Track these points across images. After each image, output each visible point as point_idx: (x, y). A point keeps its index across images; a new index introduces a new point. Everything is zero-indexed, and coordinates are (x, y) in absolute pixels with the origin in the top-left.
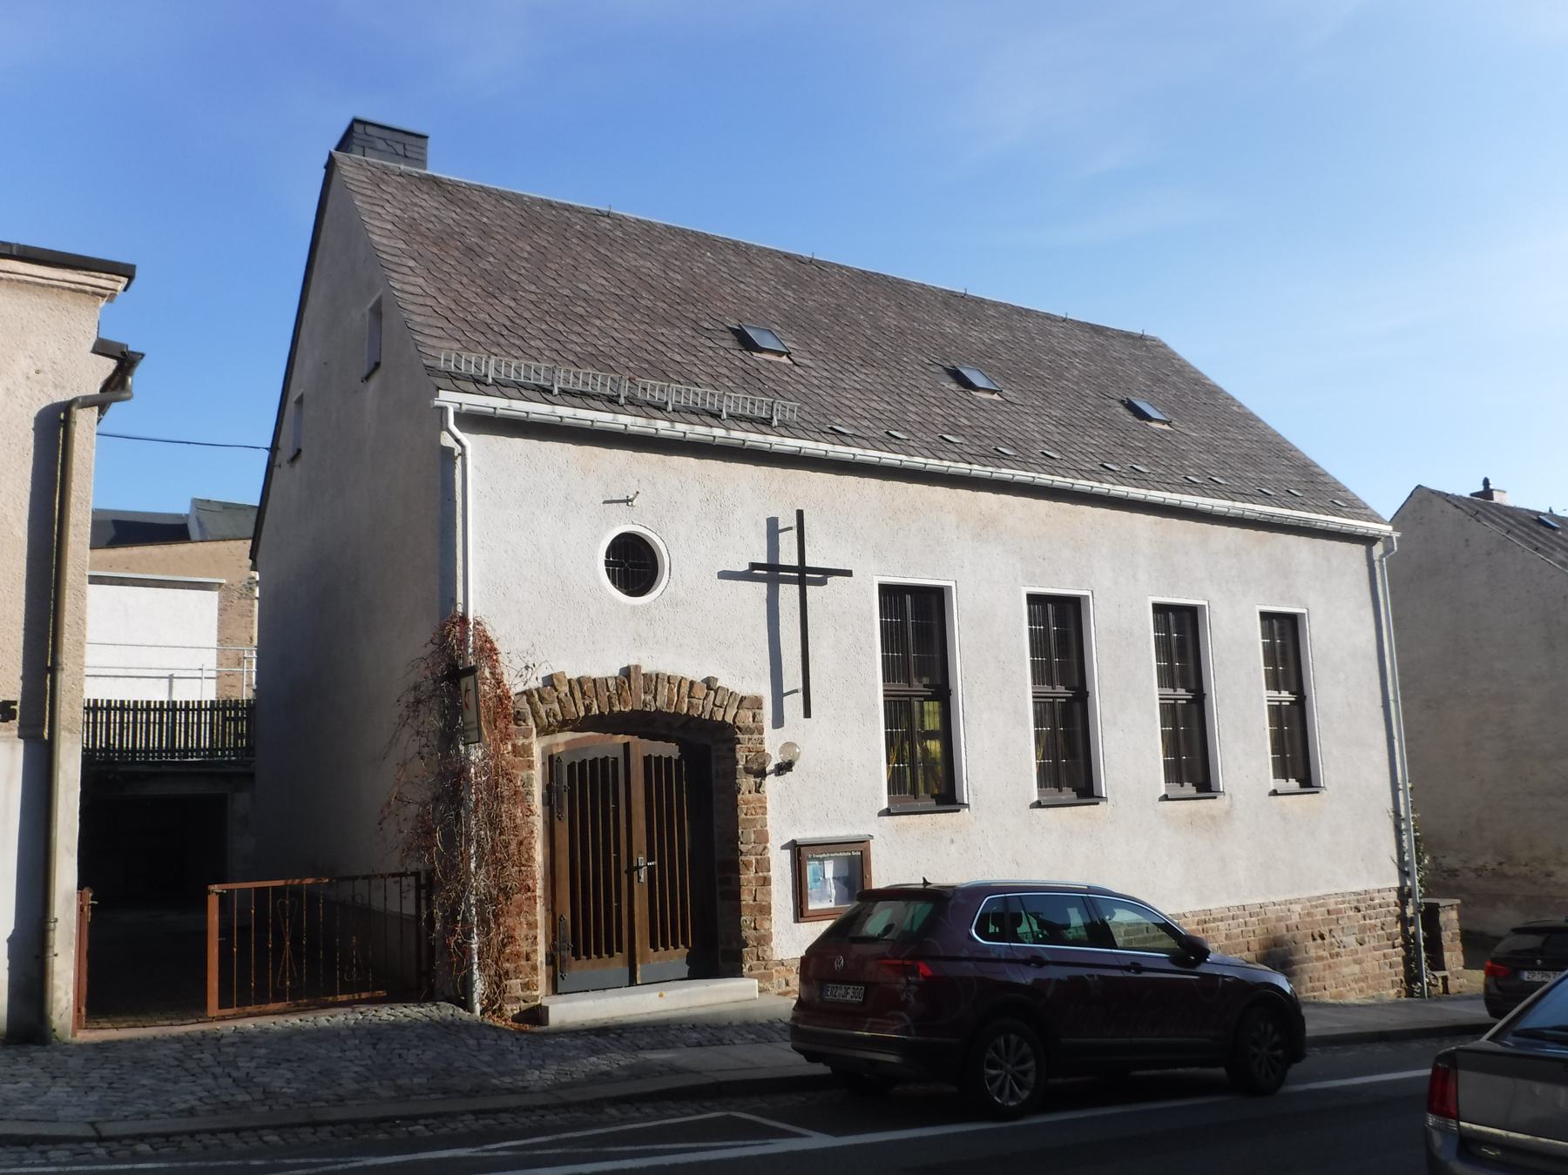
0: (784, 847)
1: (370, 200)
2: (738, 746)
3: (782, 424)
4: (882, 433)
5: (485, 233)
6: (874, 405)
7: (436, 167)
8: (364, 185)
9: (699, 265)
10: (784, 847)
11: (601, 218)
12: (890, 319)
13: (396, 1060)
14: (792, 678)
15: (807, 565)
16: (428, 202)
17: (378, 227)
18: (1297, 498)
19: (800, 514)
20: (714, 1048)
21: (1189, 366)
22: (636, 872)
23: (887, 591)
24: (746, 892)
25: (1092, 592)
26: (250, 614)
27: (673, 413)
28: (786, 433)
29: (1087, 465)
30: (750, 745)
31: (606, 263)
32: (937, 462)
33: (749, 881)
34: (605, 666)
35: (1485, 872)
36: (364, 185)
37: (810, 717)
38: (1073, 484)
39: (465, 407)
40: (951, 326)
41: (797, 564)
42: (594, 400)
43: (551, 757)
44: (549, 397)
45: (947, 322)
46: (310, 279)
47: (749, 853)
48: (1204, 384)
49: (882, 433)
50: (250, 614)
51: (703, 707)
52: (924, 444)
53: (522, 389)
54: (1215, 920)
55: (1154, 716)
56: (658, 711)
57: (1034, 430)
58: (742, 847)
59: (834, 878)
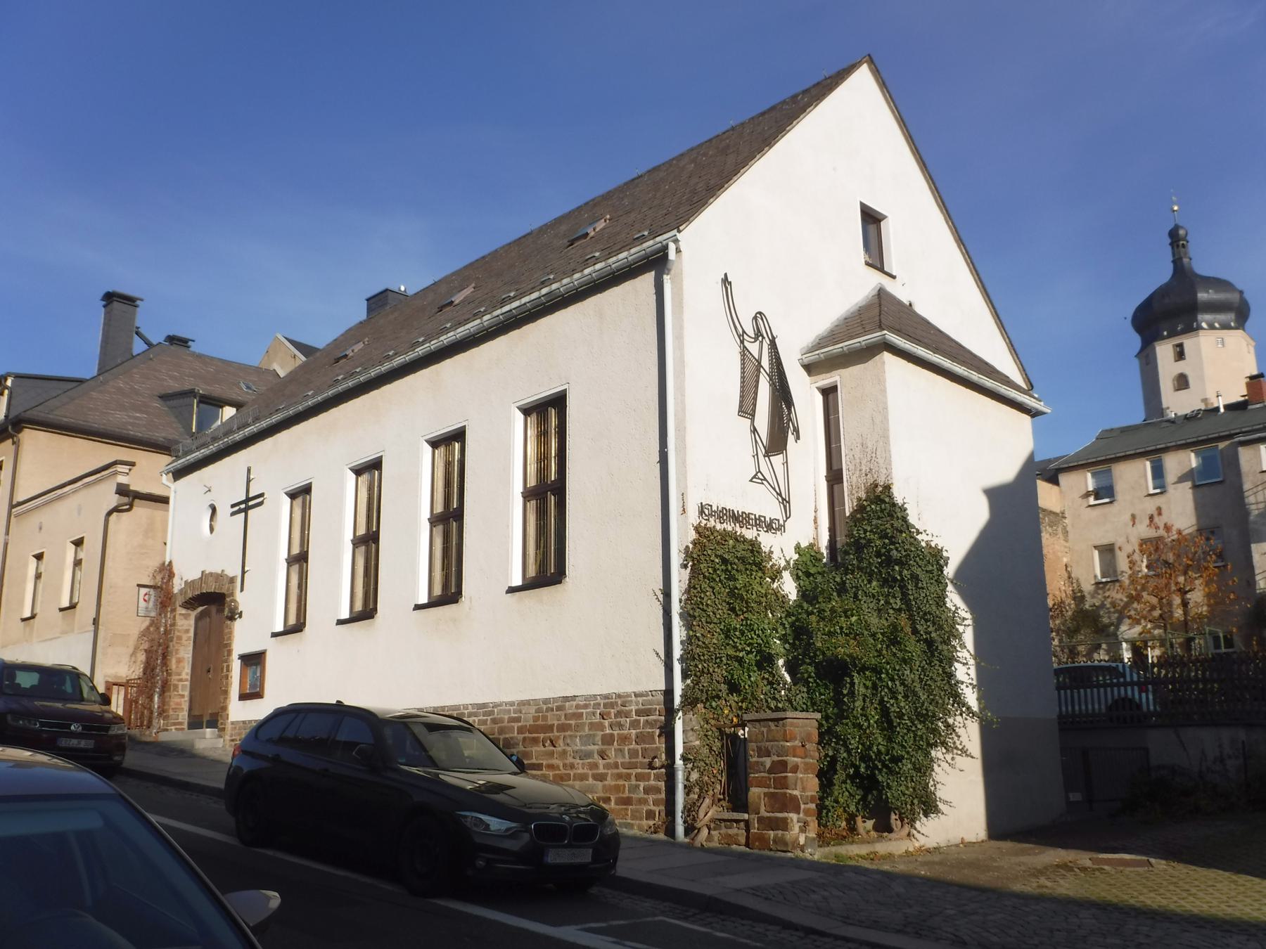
41: (1036, 460)
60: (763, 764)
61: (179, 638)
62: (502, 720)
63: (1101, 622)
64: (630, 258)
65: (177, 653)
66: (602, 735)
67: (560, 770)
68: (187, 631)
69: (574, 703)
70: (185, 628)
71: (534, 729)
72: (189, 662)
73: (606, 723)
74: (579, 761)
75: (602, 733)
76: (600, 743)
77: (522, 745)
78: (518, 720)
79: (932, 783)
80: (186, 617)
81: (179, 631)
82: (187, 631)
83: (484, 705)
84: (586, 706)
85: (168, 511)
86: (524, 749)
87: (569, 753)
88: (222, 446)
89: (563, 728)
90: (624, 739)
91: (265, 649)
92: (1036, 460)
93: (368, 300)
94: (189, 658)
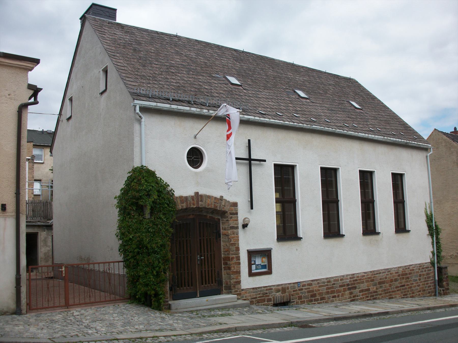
1: (101, 32)
4: (274, 113)
5: (139, 43)
6: (270, 103)
7: (120, 19)
8: (98, 27)
9: (208, 54)
11: (174, 37)
12: (270, 72)
13: (131, 321)
15: (252, 158)
16: (119, 33)
17: (105, 42)
18: (403, 136)
20: (227, 317)
21: (365, 89)
23: (275, 165)
26: (33, 168)
27: (208, 107)
28: (245, 114)
29: (339, 124)
31: (177, 53)
35: (453, 256)
36: (98, 27)
37: (253, 209)
40: (290, 75)
41: (248, 158)
42: (183, 103)
44: (169, 102)
45: (289, 74)
46: (75, 58)
48: (370, 96)
49: (274, 113)
50: (33, 168)
52: (288, 117)
57: (321, 112)
60: (445, 277)
62: (393, 273)
63: (178, 207)
71: (403, 275)
73: (419, 271)
79: (86, 266)
83: (388, 269)
84: (415, 267)
85: (276, 198)
89: (410, 274)
90: (423, 275)
91: (246, 252)
92: (248, 158)
93: (435, 129)
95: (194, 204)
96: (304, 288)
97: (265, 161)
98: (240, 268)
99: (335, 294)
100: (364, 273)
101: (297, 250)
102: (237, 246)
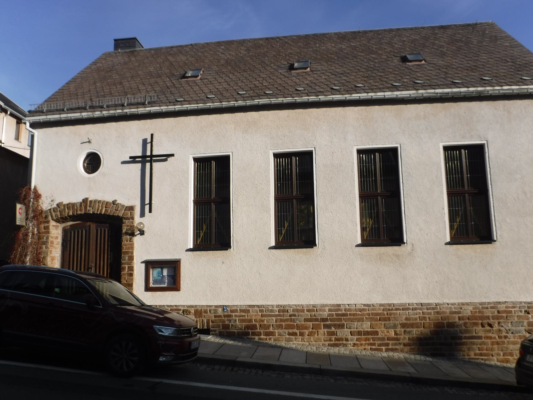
0: (142, 262)
2: (123, 224)
3: (149, 103)
10: (142, 262)
14: (147, 201)
19: (152, 135)
22: (90, 269)
24: (123, 278)
25: (315, 148)
30: (128, 224)
32: (365, 94)
33: (124, 274)
34: (77, 199)
38: (308, 99)
39: (31, 121)
43: (65, 230)
44: (145, 106)
47: (125, 264)
51: (111, 211)
53: (72, 110)
54: (396, 309)
55: (355, 204)
56: (93, 213)
58: (123, 262)
59: (167, 275)
61: (52, 242)
64: (501, 92)
65: (51, 253)
66: (528, 322)
67: (496, 339)
68: (57, 238)
69: (505, 305)
70: (55, 235)
72: (58, 259)
74: (511, 335)
75: (528, 321)
76: (527, 326)
77: (464, 326)
78: (459, 313)
80: (57, 227)
81: (52, 237)
82: (57, 238)
84: (514, 307)
86: (465, 328)
87: (503, 331)
88: (41, 120)
94: (58, 257)
95: (81, 210)
96: (234, 314)
97: (172, 155)
98: (132, 280)
99: (295, 330)
100: (364, 305)
101: (223, 263)
102: (130, 255)
